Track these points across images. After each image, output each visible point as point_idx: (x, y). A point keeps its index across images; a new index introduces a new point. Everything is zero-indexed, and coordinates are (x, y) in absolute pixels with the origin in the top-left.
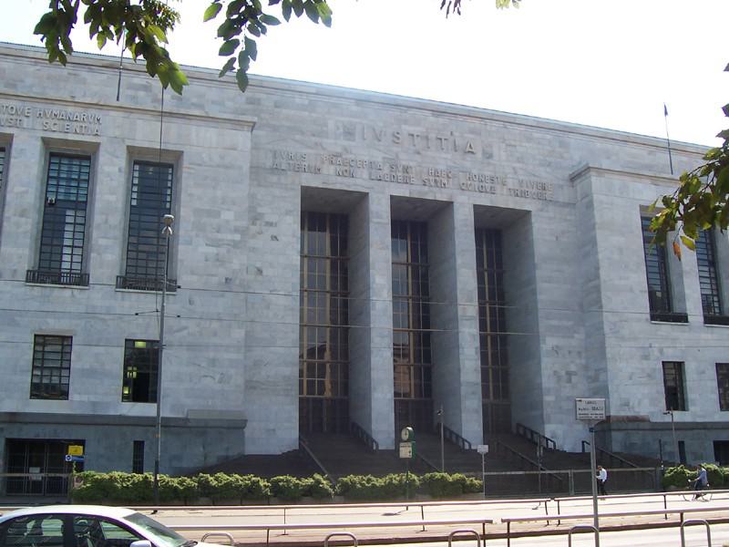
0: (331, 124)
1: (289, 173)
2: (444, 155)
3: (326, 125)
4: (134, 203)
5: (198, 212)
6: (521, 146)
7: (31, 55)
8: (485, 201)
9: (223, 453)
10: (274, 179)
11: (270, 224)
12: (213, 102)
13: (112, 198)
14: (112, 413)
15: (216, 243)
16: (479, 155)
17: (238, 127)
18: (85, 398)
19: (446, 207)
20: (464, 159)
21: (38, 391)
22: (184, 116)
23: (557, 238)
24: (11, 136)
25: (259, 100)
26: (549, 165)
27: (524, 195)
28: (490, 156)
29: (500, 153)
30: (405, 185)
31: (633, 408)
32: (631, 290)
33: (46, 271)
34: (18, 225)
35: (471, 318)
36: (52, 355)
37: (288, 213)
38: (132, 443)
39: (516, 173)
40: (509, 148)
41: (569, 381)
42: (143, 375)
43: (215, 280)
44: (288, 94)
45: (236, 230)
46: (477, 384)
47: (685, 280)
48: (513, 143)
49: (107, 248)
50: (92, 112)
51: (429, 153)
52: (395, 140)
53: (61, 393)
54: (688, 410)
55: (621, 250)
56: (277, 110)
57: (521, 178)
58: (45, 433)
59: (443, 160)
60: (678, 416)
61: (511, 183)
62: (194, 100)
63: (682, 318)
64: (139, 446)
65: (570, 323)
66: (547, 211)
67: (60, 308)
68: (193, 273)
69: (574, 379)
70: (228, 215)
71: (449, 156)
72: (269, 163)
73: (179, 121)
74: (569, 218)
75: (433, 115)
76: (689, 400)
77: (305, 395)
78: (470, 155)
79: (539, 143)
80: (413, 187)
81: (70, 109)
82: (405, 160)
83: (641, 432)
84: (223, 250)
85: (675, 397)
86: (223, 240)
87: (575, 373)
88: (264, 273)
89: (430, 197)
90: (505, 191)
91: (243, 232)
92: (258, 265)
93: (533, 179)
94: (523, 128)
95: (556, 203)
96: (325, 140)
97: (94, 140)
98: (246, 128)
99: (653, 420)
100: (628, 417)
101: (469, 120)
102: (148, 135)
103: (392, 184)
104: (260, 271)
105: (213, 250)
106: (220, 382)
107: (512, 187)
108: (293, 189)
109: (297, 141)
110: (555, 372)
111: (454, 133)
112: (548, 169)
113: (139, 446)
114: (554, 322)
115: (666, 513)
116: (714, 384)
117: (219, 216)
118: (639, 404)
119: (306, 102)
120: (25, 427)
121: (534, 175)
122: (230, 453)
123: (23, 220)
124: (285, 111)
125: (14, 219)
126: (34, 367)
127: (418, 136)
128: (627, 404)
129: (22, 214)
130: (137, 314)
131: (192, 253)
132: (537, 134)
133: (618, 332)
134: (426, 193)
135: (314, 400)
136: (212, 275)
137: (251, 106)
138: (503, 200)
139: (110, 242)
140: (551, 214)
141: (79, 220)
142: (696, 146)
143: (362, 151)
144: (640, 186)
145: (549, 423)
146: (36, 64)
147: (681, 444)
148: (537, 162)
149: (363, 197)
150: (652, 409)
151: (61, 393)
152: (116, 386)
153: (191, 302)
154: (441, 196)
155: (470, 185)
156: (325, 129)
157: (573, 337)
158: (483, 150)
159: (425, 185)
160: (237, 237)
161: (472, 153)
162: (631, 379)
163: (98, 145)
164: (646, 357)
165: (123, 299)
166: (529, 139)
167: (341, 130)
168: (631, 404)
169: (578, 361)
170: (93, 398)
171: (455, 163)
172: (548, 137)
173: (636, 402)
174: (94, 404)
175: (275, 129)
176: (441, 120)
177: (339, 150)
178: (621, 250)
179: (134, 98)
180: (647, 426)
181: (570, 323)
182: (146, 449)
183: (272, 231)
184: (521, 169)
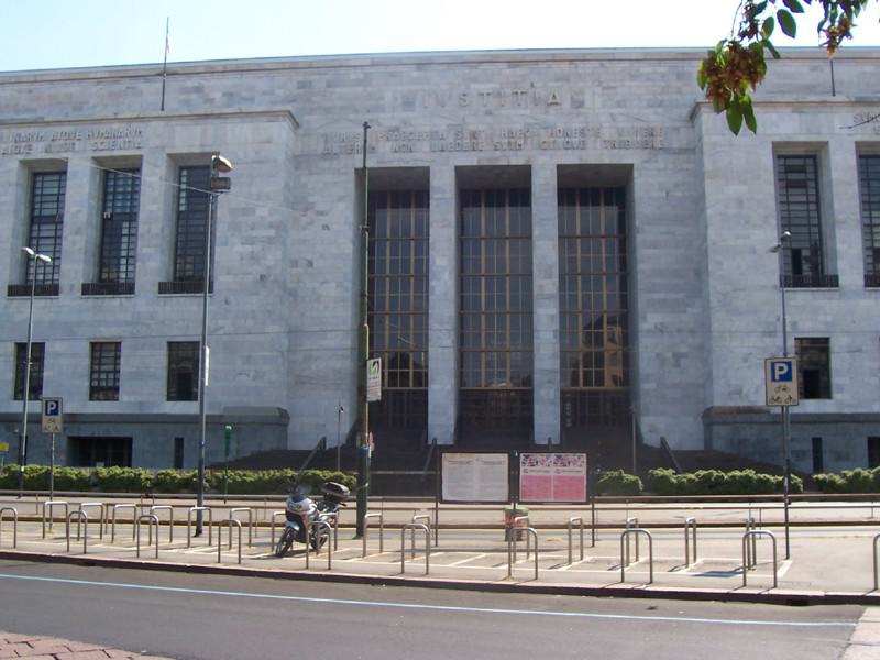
0: (388, 96)
1: (342, 156)
2: (522, 112)
3: (382, 98)
4: (182, 208)
5: (233, 211)
6: (623, 86)
7: (92, 76)
8: (571, 158)
9: (255, 449)
10: (326, 164)
11: (321, 213)
12: (264, 93)
13: (154, 207)
14: (156, 411)
15: (250, 241)
16: (567, 105)
17: (272, 119)
18: (132, 399)
19: (525, 172)
20: (547, 113)
21: (96, 392)
22: (219, 116)
23: (667, 193)
25: (311, 82)
26: (661, 104)
27: (625, 145)
28: (581, 104)
29: (594, 101)
30: (473, 153)
31: (747, 396)
32: (753, 251)
33: (24, 288)
34: (74, 243)
35: (549, 297)
36: (29, 358)
37: (341, 199)
38: (173, 439)
39: (614, 120)
40: (606, 92)
41: (677, 365)
42: (183, 377)
44: (342, 71)
45: (271, 226)
46: (553, 371)
47: (837, 231)
48: (613, 84)
49: (151, 257)
50: (135, 126)
51: (503, 112)
52: (462, 102)
55: (740, 203)
56: (331, 89)
57: (621, 125)
59: (518, 117)
60: (812, 406)
61: (607, 134)
62: (245, 94)
63: (832, 282)
64: (179, 442)
65: (681, 295)
66: (656, 161)
68: (229, 273)
69: (683, 362)
70: (262, 212)
71: (528, 112)
72: (320, 149)
73: (216, 121)
74: (685, 166)
75: (510, 67)
77: (386, 387)
78: (554, 107)
79: (648, 79)
80: (482, 154)
81: (116, 126)
82: (473, 124)
83: (755, 426)
84: (257, 248)
85: (104, 388)
87: (685, 356)
88: (315, 265)
89: (503, 162)
90: (598, 145)
91: (280, 227)
92: (309, 257)
93: (638, 124)
94: (626, 64)
95: (666, 150)
96: (382, 115)
97: (137, 152)
98: (281, 118)
100: (739, 408)
101: (554, 65)
102: (189, 140)
103: (459, 154)
104: (310, 264)
105: (248, 248)
106: (254, 379)
107: (607, 138)
108: (345, 173)
109: (351, 121)
110: (658, 355)
112: (660, 110)
113: (179, 442)
114: (658, 296)
115: (787, 524)
117: (254, 211)
119: (361, 76)
120: (83, 426)
122: (263, 449)
123: (78, 237)
124: (338, 90)
125: (70, 238)
126: (92, 372)
127: (488, 94)
128: (739, 392)
129: (78, 232)
130: (180, 316)
131: (228, 254)
132: (645, 69)
134: (497, 159)
135: (591, 393)
136: (248, 274)
137: (302, 91)
138: (596, 154)
139: (152, 250)
140: (662, 166)
143: (421, 122)
144: (774, 116)
146: (98, 83)
147: (817, 442)
148: (645, 103)
149: (426, 172)
152: (161, 385)
153: (227, 302)
154: (517, 160)
155: (554, 142)
156: (381, 102)
157: (685, 312)
158: (572, 98)
159: (496, 150)
160: (272, 233)
161: (556, 104)
162: (746, 360)
163: (141, 157)
165: (165, 304)
166: (634, 77)
167: (399, 101)
168: (745, 391)
169: (690, 340)
170: (140, 399)
172: (662, 69)
173: (753, 390)
174: (141, 404)
175: (328, 110)
176: (519, 71)
177: (395, 123)
178: (740, 203)
179: (187, 102)
180: (764, 418)
181: (681, 295)
182: (185, 445)
183: (324, 220)
184: (622, 114)
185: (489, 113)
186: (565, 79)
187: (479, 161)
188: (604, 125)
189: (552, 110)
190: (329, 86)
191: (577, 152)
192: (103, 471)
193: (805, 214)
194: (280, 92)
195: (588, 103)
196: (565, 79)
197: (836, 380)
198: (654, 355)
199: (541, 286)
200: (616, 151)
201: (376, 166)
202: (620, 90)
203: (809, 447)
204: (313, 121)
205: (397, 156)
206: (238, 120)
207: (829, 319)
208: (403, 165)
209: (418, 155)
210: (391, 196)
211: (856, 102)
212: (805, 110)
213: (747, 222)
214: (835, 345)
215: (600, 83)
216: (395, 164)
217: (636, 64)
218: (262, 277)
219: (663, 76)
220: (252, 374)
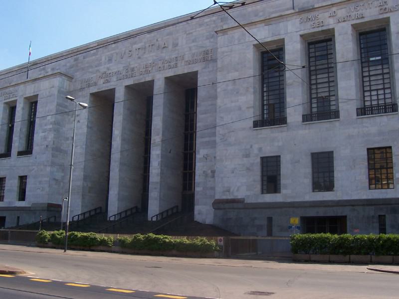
8: (170, 73)
10: (80, 93)
16: (170, 47)
19: (151, 84)
24: (388, 18)
27: (195, 62)
32: (240, 108)
43: (43, 147)
46: (157, 183)
48: (191, 31)
51: (145, 56)
53: (330, 187)
54: (280, 192)
57: (193, 51)
58: (331, 212)
60: (269, 198)
67: (271, 141)
76: (282, 185)
78: (165, 49)
81: (11, 89)
86: (46, 129)
99: (248, 201)
100: (227, 200)
102: (29, 90)
105: (44, 134)
110: (204, 172)
111: (159, 40)
113: (18, 217)
116: (308, 170)
118: (238, 190)
121: (203, 47)
127: (139, 49)
128: (229, 191)
132: (207, 20)
133: (226, 140)
138: (182, 69)
141: (385, 71)
142: (66, 52)
145: (198, 205)
147: (270, 220)
150: (248, 193)
151: (330, 187)
154: (148, 79)
162: (233, 173)
164: (247, 156)
166: (201, 25)
168: (231, 190)
171: (157, 57)
172: (214, 18)
173: (236, 189)
175: (83, 69)
177: (105, 70)
184: (194, 46)
185: (139, 58)
186: (170, 34)
187: (134, 82)
188: (186, 53)
189: (164, 50)
190: (84, 58)
191: (173, 70)
192: (185, 240)
193: (372, 83)
194: (68, 65)
195: (180, 44)
196: (170, 34)
197: (284, 181)
198: (202, 172)
199: (154, 140)
200: (190, 66)
201: (97, 91)
202: (194, 34)
203: (265, 222)
204: (78, 75)
205: (104, 85)
206: (45, 79)
207: (280, 144)
208: (107, 89)
209: (112, 83)
210: (104, 101)
211: (299, 12)
212: (272, 23)
213: (237, 93)
214: (283, 160)
215: (186, 32)
216: (103, 89)
217: (202, 19)
218: (47, 146)
219: (214, 21)
220: (41, 188)
